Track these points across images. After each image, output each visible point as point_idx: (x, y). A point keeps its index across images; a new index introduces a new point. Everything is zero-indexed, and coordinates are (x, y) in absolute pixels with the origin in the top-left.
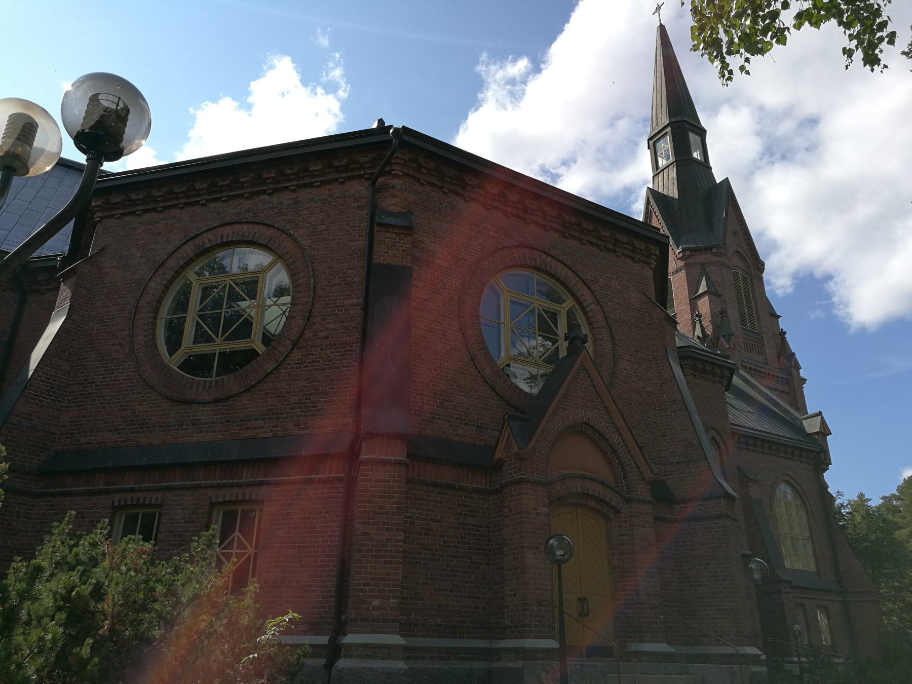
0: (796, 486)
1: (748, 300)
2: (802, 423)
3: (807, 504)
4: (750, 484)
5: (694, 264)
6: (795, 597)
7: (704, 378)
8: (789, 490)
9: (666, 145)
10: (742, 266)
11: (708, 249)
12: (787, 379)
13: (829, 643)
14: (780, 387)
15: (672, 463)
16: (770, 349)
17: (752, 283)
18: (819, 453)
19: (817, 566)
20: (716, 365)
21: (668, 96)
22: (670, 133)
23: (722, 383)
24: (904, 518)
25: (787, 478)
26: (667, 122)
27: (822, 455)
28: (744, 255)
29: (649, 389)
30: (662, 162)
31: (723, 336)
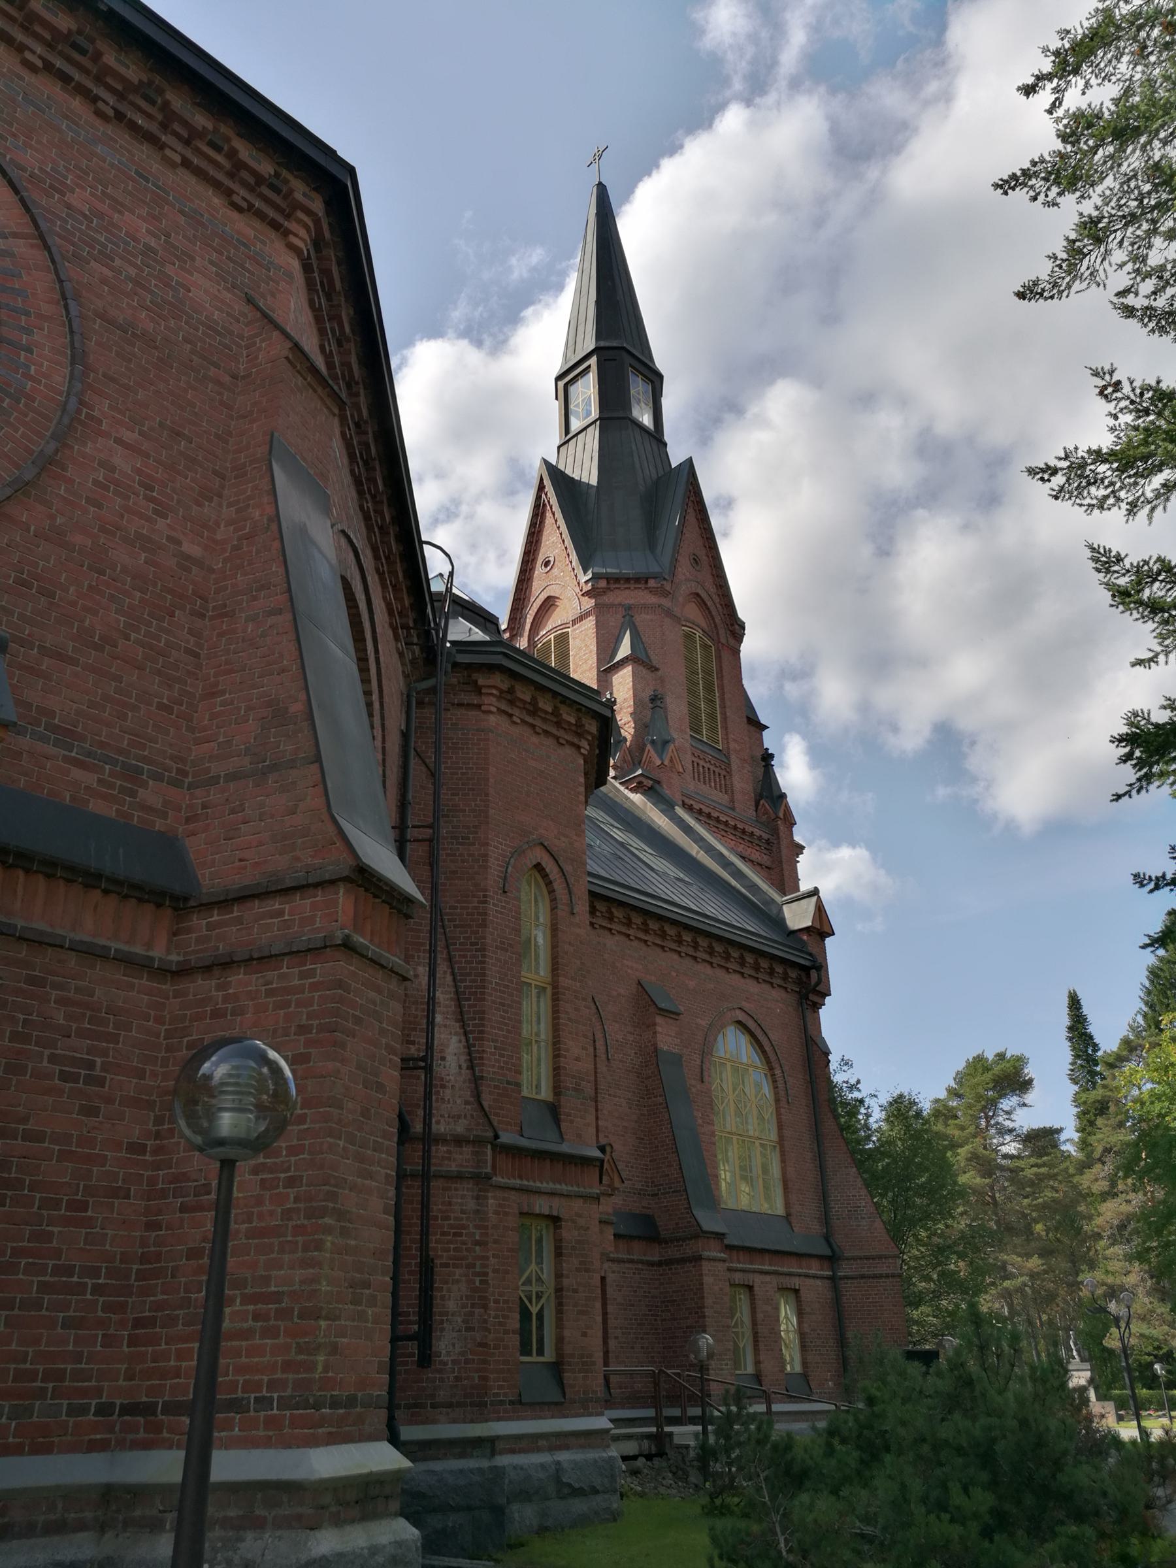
0: (758, 1033)
1: (709, 688)
2: (781, 910)
3: (778, 1072)
4: (659, 1020)
5: (612, 606)
6: (729, 1270)
7: (533, 726)
8: (744, 1041)
9: (587, 390)
10: (704, 625)
11: (640, 580)
12: (768, 842)
13: (798, 1368)
14: (756, 856)
15: (214, 780)
16: (743, 782)
17: (719, 658)
18: (806, 970)
19: (787, 1205)
20: (565, 700)
21: (598, 302)
22: (594, 368)
23: (579, 747)
24: (962, 1128)
25: (741, 1016)
26: (592, 347)
27: (814, 974)
28: (709, 603)
29: (192, 549)
30: (576, 425)
31: (653, 742)
